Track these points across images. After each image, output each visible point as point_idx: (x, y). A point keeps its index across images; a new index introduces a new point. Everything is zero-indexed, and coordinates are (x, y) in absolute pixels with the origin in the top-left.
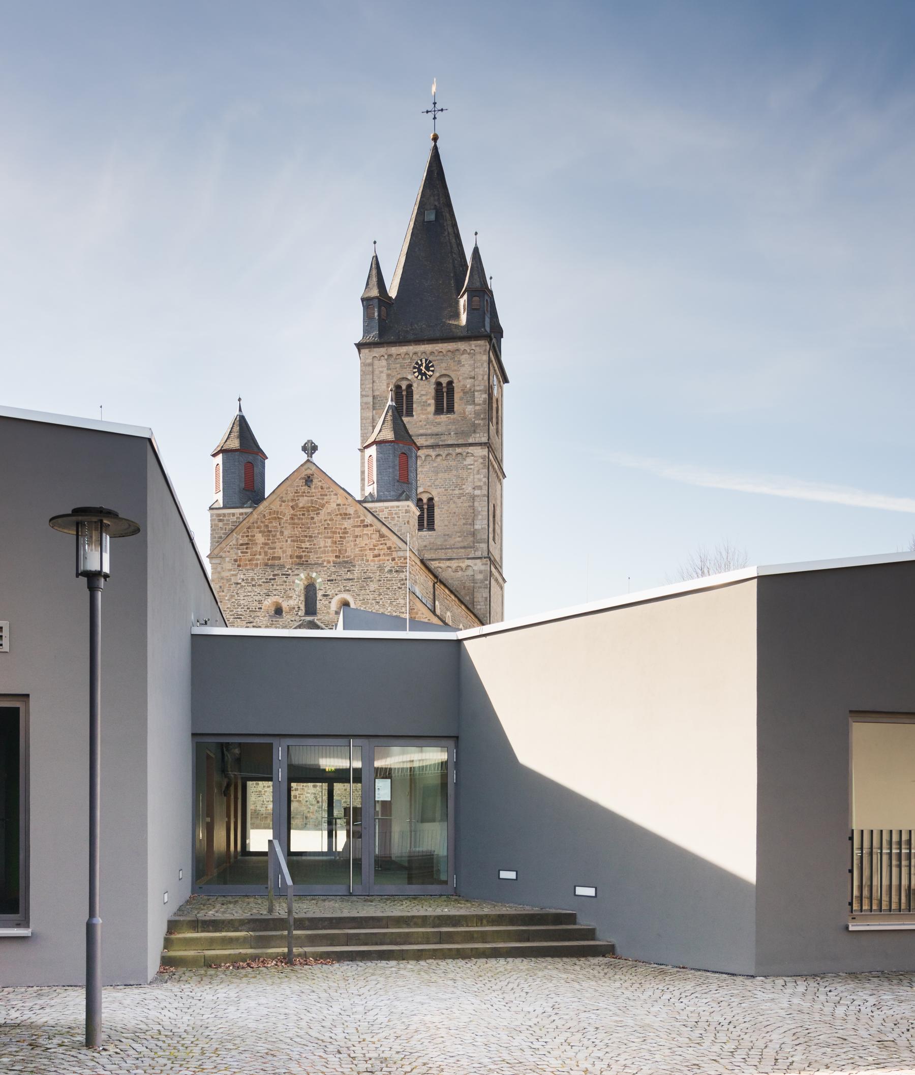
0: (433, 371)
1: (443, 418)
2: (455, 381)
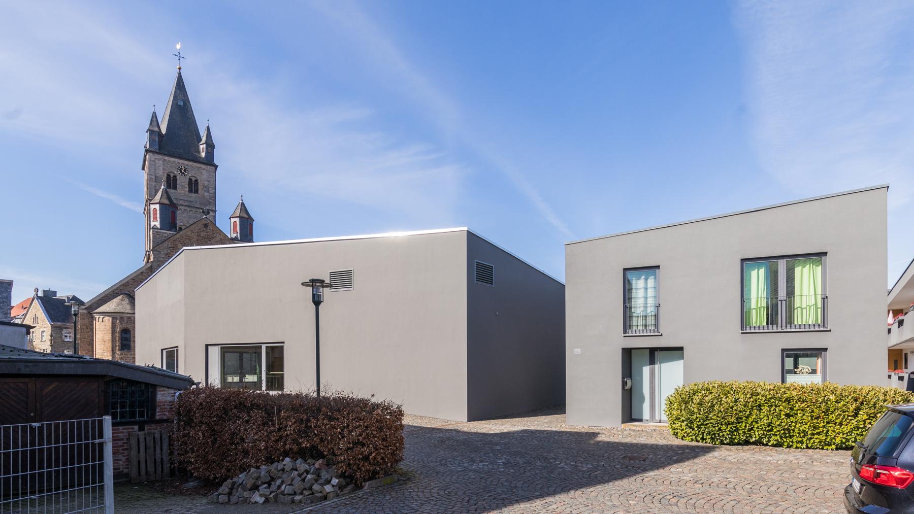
1: (193, 195)
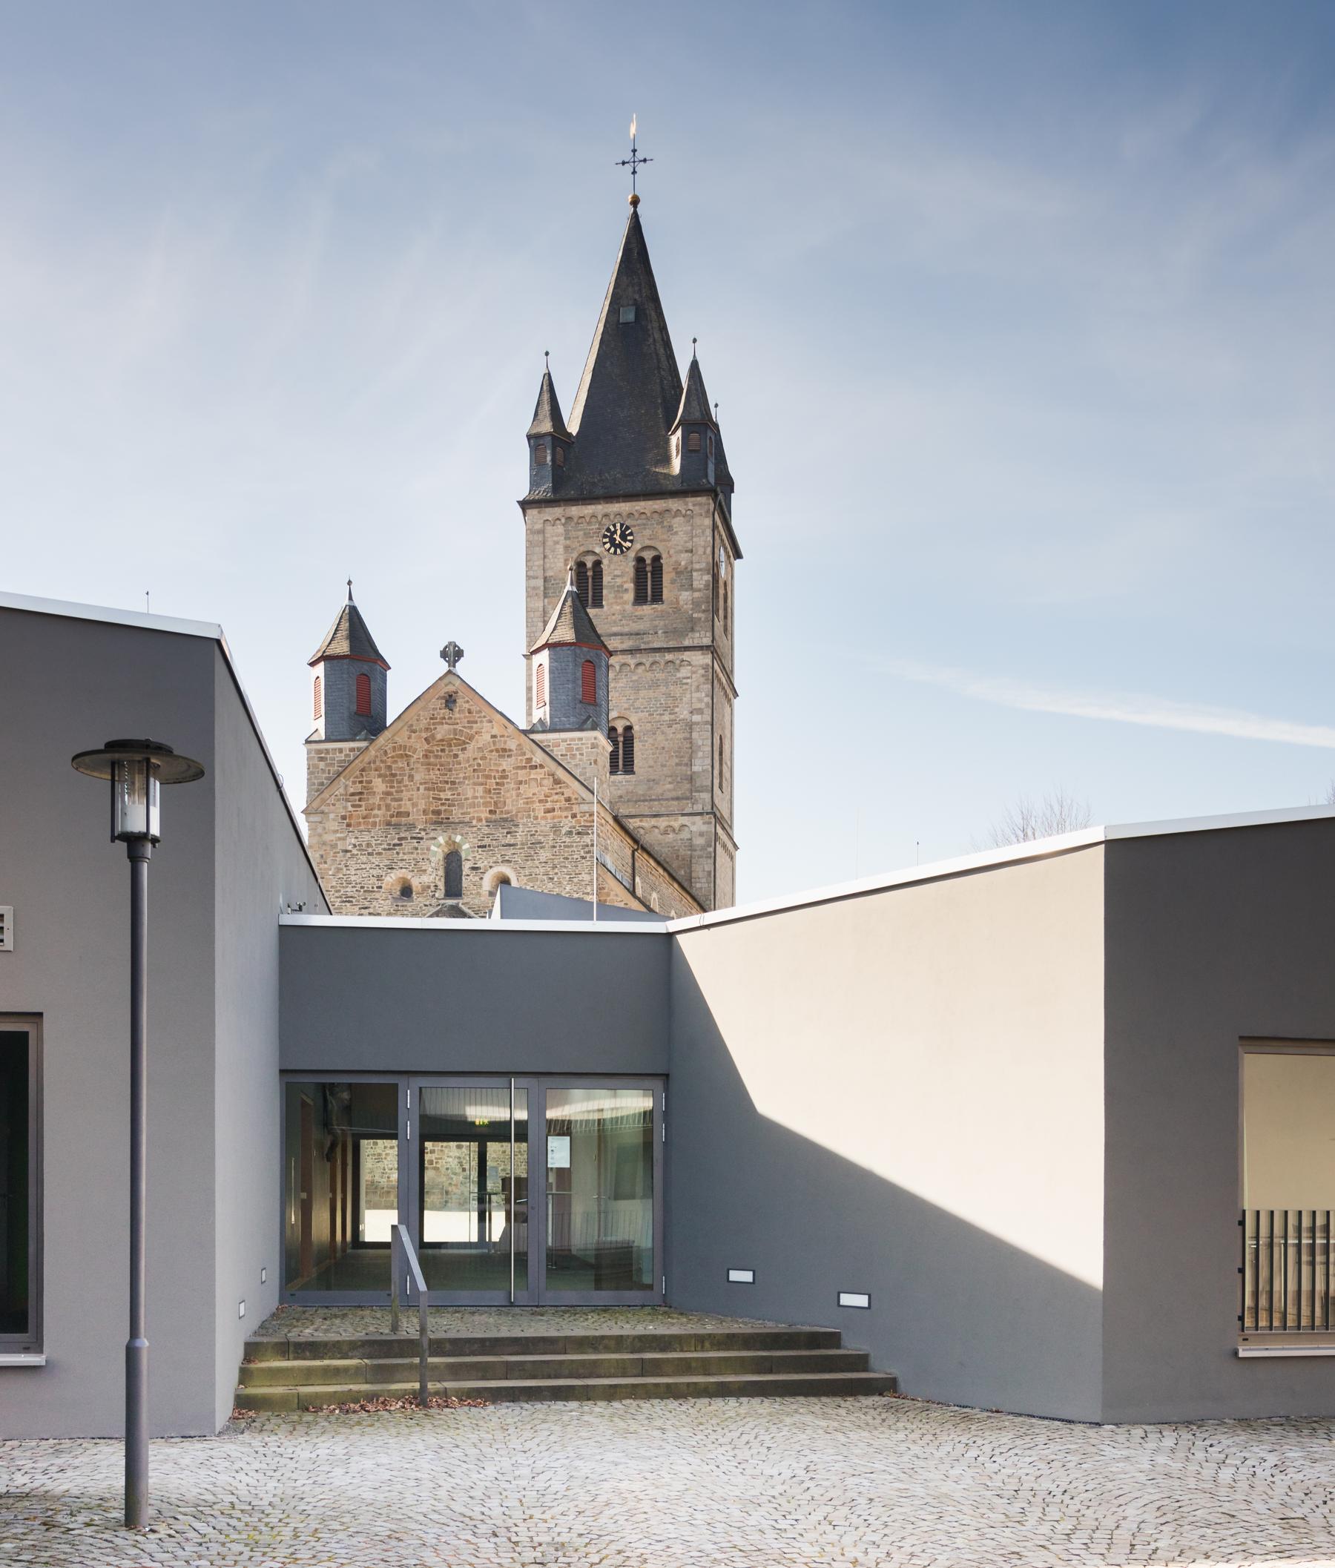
0: (631, 541)
1: (647, 609)
2: (664, 556)
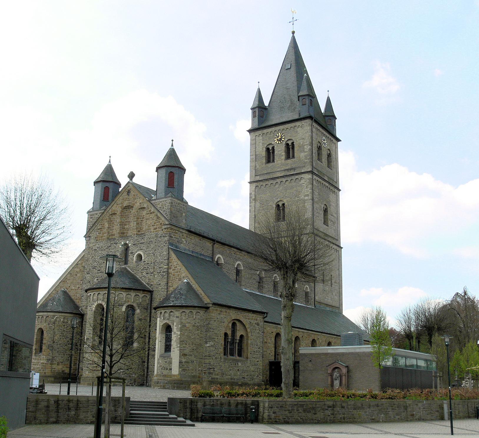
1: (289, 161)
